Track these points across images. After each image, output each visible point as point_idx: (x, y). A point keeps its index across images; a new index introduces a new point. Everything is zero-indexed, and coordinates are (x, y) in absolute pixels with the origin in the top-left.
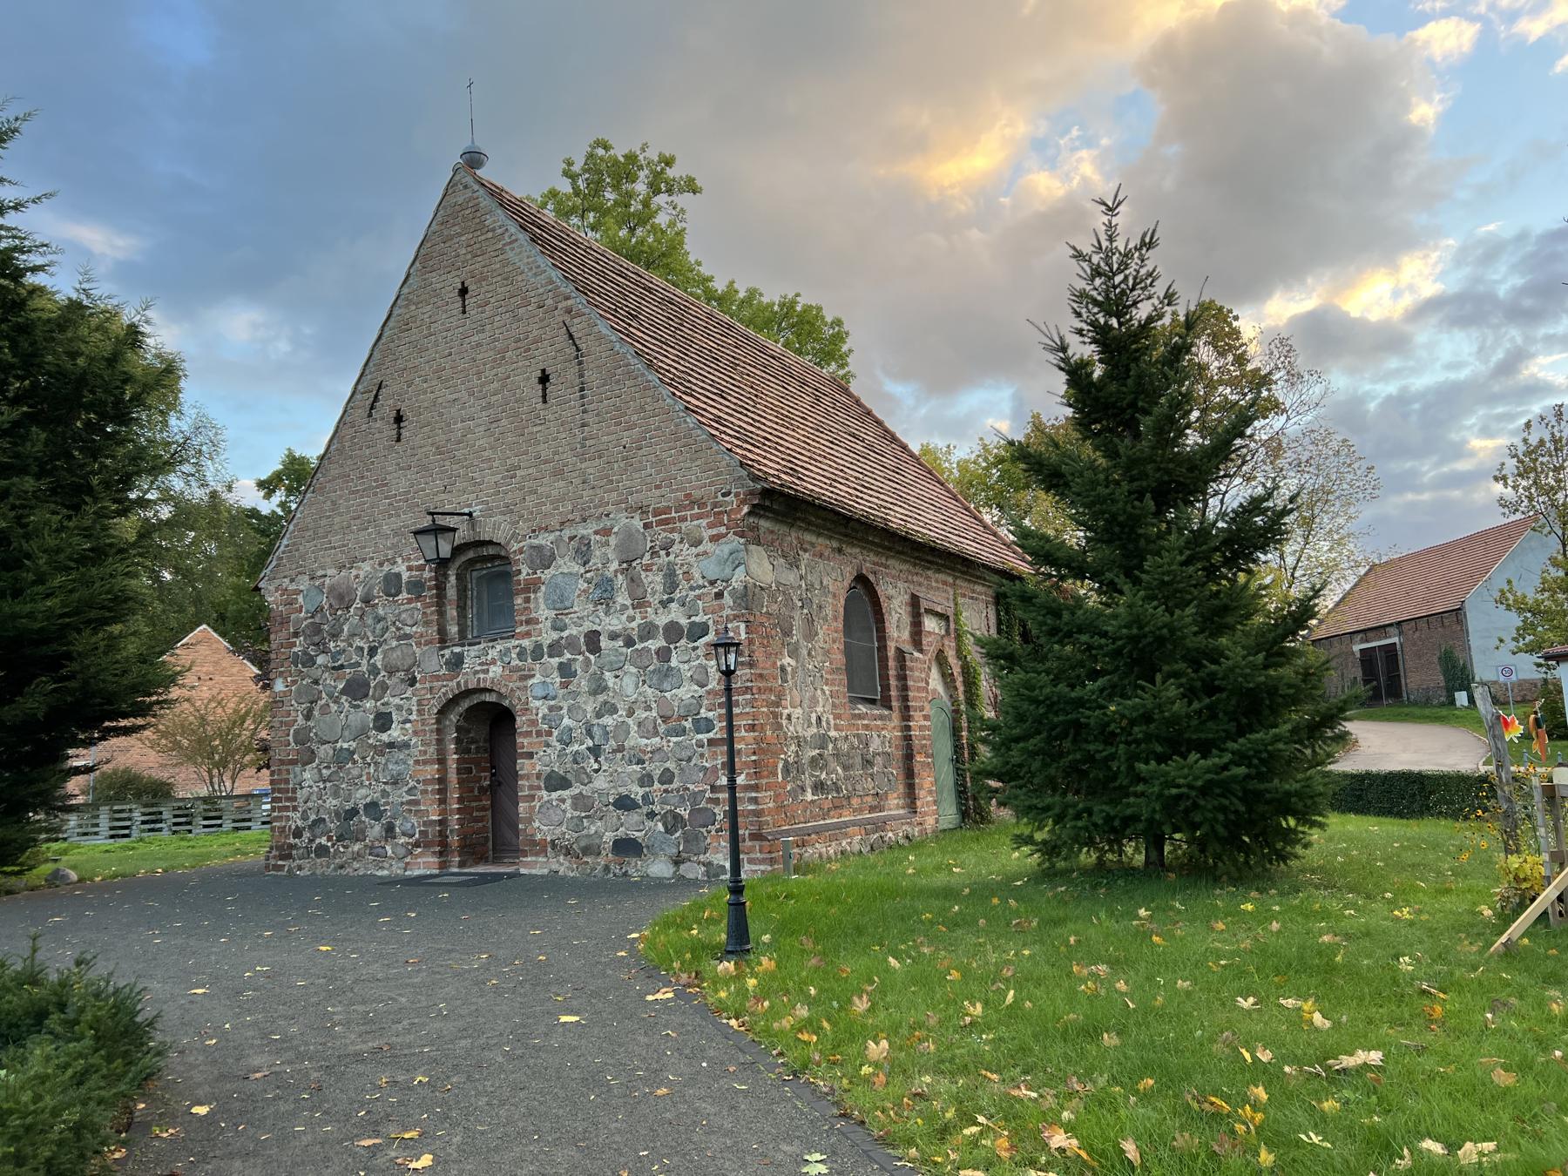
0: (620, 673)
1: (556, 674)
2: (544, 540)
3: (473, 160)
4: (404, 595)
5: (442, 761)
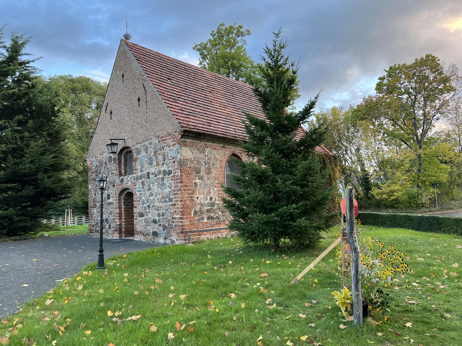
0: (154, 184)
1: (141, 185)
2: (138, 146)
3: (127, 37)
4: (112, 162)
5: (120, 208)
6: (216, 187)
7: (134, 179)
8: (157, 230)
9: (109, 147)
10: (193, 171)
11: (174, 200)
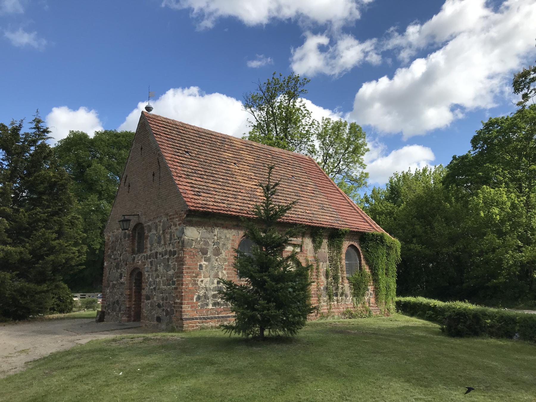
1: (150, 265)
4: (127, 239)
6: (225, 269)
7: (144, 258)
8: (160, 316)
9: (121, 223)
10: (198, 252)
11: (176, 283)
